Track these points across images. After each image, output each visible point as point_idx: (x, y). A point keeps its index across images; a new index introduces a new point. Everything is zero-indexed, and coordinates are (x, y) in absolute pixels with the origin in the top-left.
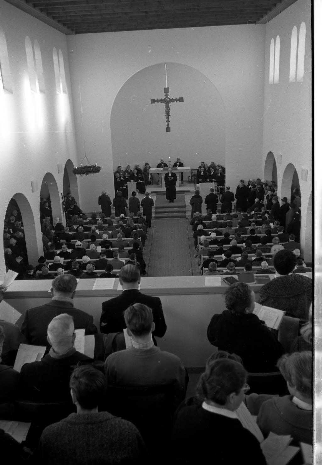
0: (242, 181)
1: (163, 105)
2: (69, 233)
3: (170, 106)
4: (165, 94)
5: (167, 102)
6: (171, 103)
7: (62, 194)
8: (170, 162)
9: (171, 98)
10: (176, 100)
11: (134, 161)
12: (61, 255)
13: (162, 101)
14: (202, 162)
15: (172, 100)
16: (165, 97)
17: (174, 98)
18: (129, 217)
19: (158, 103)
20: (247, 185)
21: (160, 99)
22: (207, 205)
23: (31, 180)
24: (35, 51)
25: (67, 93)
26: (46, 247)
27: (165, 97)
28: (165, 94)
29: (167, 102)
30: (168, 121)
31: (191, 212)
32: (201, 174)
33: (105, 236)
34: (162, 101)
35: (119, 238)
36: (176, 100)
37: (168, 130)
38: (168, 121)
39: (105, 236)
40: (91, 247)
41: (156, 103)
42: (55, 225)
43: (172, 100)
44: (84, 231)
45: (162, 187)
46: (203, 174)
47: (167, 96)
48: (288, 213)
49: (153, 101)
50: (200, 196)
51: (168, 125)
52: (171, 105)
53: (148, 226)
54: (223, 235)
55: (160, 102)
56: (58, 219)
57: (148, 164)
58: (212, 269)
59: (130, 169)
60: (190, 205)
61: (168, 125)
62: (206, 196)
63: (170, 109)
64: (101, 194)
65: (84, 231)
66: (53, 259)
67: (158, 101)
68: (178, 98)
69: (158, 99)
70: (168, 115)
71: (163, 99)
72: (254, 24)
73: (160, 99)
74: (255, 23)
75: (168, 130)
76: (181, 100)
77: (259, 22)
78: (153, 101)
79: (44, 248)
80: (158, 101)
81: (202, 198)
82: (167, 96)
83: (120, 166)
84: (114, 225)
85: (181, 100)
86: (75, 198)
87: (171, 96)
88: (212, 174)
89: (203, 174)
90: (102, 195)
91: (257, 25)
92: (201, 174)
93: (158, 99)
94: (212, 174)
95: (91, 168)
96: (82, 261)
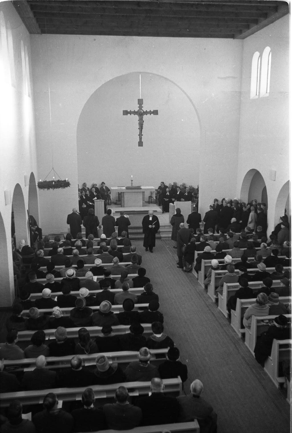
0: (216, 200)
1: (137, 117)
2: (44, 257)
3: (144, 119)
4: (138, 106)
5: (141, 114)
6: (145, 115)
7: (27, 210)
8: (132, 181)
9: (145, 111)
10: (150, 113)
11: (93, 180)
12: (48, 286)
13: (135, 113)
14: (161, 182)
15: (146, 113)
16: (138, 109)
17: (148, 111)
18: (72, 240)
19: (131, 115)
20: (220, 203)
21: (133, 110)
22: (189, 224)
23: (5, 190)
24: (8, 38)
25: (31, 97)
26: (17, 276)
27: (138, 109)
28: (138, 106)
29: (141, 114)
30: (141, 135)
31: (171, 233)
32: (167, 194)
33: (98, 262)
34: (135, 113)
35: (115, 263)
36: (150, 113)
37: (141, 144)
38: (141, 135)
39: (98, 262)
40: (86, 275)
41: (129, 115)
42: (21, 249)
43: (146, 113)
44: (44, 256)
45: (124, 207)
46: (169, 194)
47: (141, 107)
48: (280, 232)
49: (126, 113)
50: (182, 215)
51: (141, 138)
52: (145, 117)
53: (148, 248)
54: (72, 255)
55: (133, 114)
56: (23, 241)
57: (105, 183)
58: (263, 302)
59: (87, 186)
60: (170, 224)
61: (141, 138)
62: (189, 215)
63: (143, 122)
64: (71, 212)
65: (44, 256)
66: (41, 292)
67: (130, 113)
68: (152, 111)
69: (131, 111)
70: (141, 127)
71: (136, 110)
72: (232, 39)
73: (133, 111)
74: (233, 37)
75: (141, 144)
76: (156, 112)
77: (241, 35)
78: (126, 113)
79: (14, 277)
80: (130, 113)
81: (183, 217)
82: (141, 107)
83: (85, 183)
84: (94, 247)
85: (156, 112)
86: (34, 216)
87: (144, 109)
88: (178, 193)
89: (169, 194)
90: (72, 213)
91: (235, 40)
92: (167, 194)
93: (131, 111)
94: (178, 193)
95: (52, 183)
96: (78, 295)
